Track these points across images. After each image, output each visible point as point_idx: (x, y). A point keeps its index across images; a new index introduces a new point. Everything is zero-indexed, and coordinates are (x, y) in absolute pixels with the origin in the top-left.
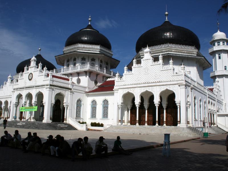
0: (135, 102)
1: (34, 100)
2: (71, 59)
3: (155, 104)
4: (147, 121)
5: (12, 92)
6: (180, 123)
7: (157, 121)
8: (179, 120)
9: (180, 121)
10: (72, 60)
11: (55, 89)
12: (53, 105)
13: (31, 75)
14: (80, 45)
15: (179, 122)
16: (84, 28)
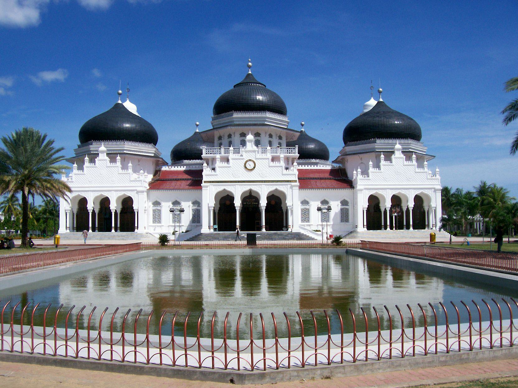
10: (226, 137)
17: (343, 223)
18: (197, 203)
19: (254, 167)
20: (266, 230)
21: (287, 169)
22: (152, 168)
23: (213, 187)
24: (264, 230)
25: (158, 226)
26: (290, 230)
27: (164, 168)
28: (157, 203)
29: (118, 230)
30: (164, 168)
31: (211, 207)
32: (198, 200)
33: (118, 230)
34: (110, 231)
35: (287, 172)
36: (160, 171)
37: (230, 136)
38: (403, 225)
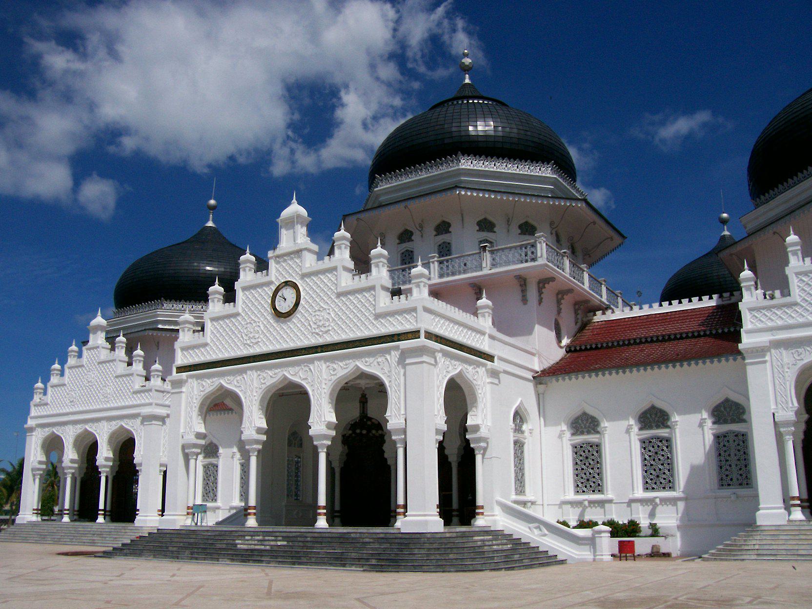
0: (384, 448)
1: (254, 422)
2: (421, 227)
3: (97, 467)
4: (324, 508)
5: (540, 304)
6: (404, 514)
7: (454, 510)
8: (401, 501)
9: (405, 506)
10: (430, 231)
11: (446, 354)
12: (260, 447)
13: (289, 293)
14: (467, 164)
15: (402, 510)
16: (451, 97)
17: (726, 492)
18: (730, 412)
19: (297, 304)
20: (331, 521)
21: (396, 292)
22: (568, 321)
23: (323, 366)
24: (322, 523)
25: (664, 501)
26: (480, 522)
27: (599, 317)
28: (584, 423)
29: (455, 520)
30: (599, 317)
31: (787, 424)
32: (735, 397)
33: (455, 520)
34: (94, 519)
35: (401, 302)
36: (589, 322)
37: (443, 228)
38: (315, 506)
